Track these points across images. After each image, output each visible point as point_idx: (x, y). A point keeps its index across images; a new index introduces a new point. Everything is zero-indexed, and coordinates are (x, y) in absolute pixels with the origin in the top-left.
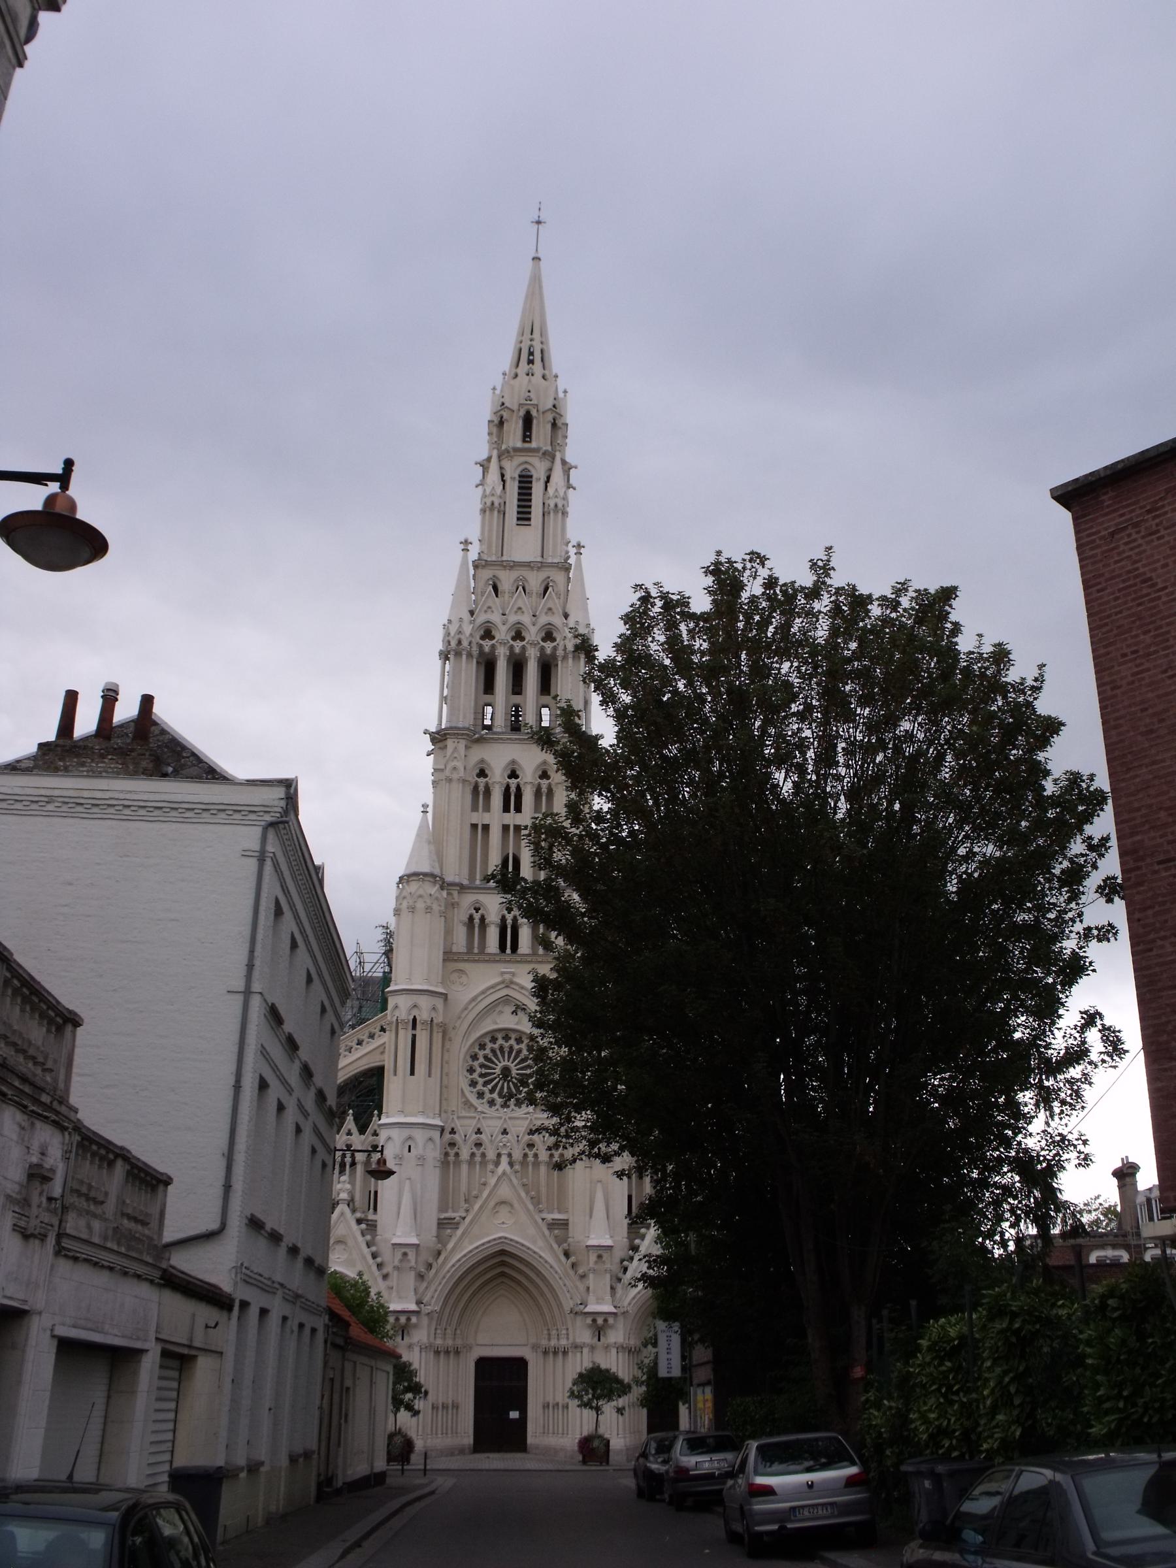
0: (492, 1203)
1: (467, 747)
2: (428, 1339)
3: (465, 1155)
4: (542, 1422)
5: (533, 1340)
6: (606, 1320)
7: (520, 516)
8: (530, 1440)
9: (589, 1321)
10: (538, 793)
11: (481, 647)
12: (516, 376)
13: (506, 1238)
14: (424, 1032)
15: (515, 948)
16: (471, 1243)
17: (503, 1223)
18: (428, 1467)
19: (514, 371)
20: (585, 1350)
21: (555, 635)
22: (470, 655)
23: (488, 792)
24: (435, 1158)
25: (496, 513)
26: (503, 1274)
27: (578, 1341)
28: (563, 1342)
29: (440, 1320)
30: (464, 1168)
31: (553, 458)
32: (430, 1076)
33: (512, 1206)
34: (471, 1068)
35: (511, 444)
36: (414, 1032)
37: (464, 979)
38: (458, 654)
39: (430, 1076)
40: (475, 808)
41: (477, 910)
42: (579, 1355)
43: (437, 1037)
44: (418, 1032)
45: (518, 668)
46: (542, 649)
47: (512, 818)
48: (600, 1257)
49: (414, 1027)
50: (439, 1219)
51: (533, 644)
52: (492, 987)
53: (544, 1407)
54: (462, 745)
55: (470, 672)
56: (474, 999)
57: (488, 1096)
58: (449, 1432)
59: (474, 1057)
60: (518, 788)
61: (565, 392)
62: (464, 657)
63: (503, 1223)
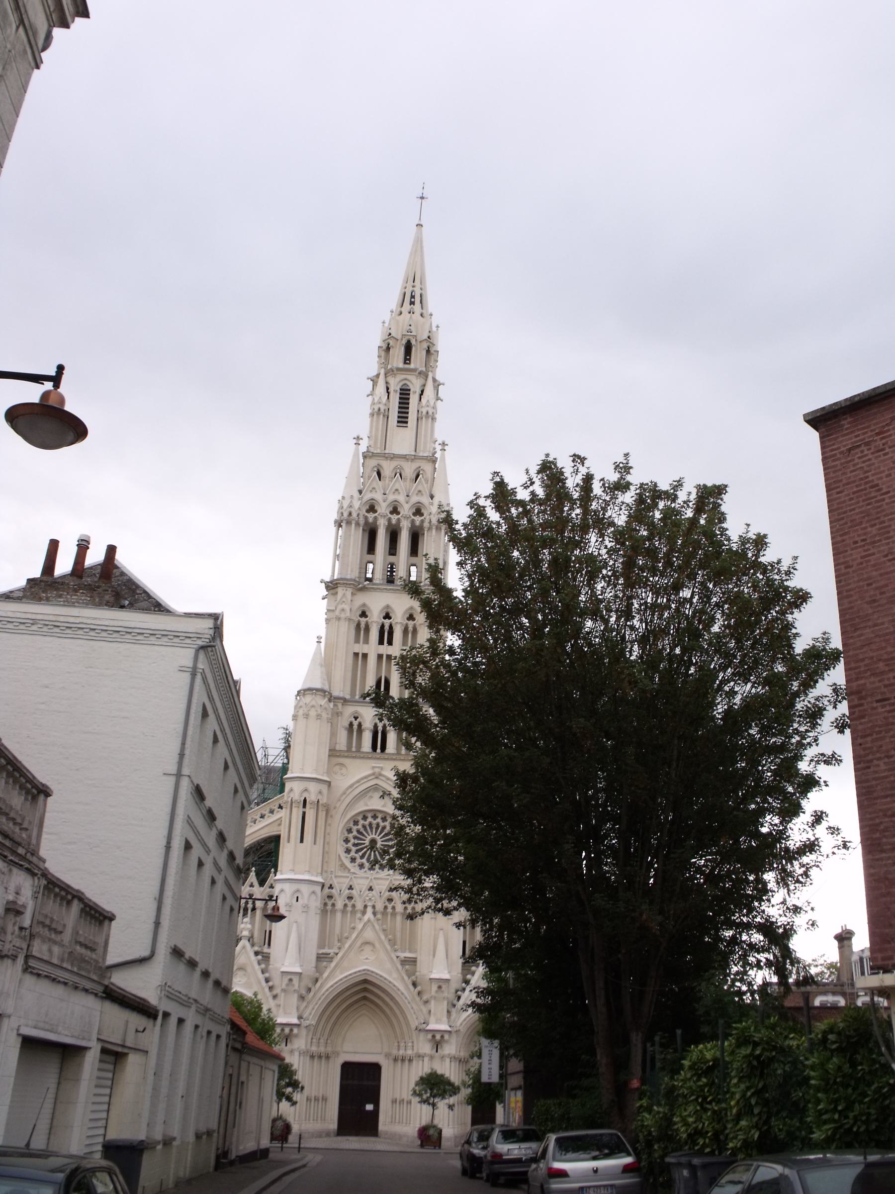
0: (359, 943)
1: (353, 594)
2: (306, 1046)
3: (339, 905)
4: (390, 1114)
5: (386, 1050)
6: (442, 1037)
7: (401, 401)
8: (381, 1127)
9: (430, 1036)
10: (405, 631)
11: (366, 518)
12: (401, 313)
13: (368, 970)
14: (312, 810)
15: (383, 748)
16: (341, 973)
17: (367, 959)
18: (302, 1146)
19: (399, 309)
20: (426, 1059)
21: (423, 511)
22: (357, 524)
23: (367, 629)
24: (316, 907)
25: (382, 416)
26: (365, 998)
27: (421, 1051)
28: (409, 1052)
29: (314, 1034)
30: (339, 915)
31: (427, 377)
32: (315, 843)
33: (374, 945)
34: (347, 839)
35: (395, 365)
36: (304, 810)
37: (344, 771)
38: (349, 523)
39: (315, 843)
40: (357, 641)
41: (356, 718)
42: (421, 1062)
43: (322, 814)
44: (307, 810)
45: (393, 536)
46: (413, 522)
47: (385, 649)
48: (440, 987)
49: (304, 806)
50: (318, 954)
51: (406, 518)
52: (365, 777)
53: (393, 1102)
54: (349, 592)
55: (358, 537)
56: (351, 786)
57: (359, 861)
58: (319, 1119)
59: (350, 831)
60: (391, 627)
61: (438, 327)
62: (353, 525)
63: (367, 959)
